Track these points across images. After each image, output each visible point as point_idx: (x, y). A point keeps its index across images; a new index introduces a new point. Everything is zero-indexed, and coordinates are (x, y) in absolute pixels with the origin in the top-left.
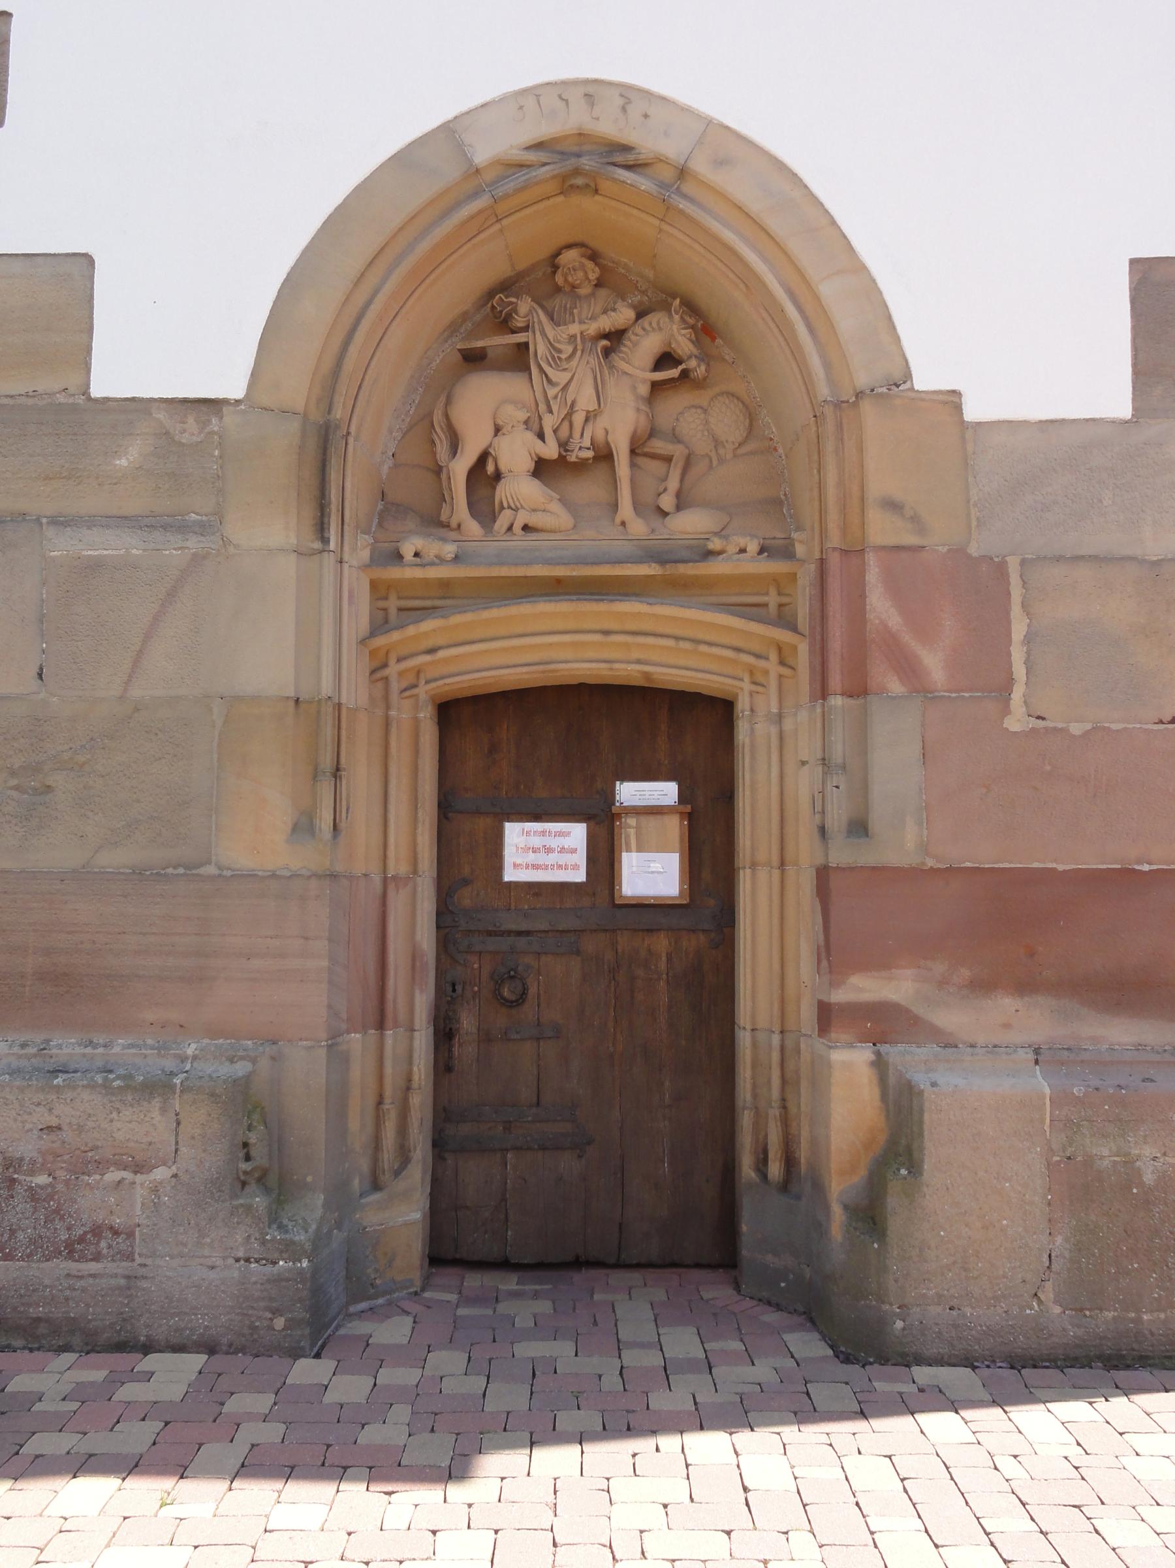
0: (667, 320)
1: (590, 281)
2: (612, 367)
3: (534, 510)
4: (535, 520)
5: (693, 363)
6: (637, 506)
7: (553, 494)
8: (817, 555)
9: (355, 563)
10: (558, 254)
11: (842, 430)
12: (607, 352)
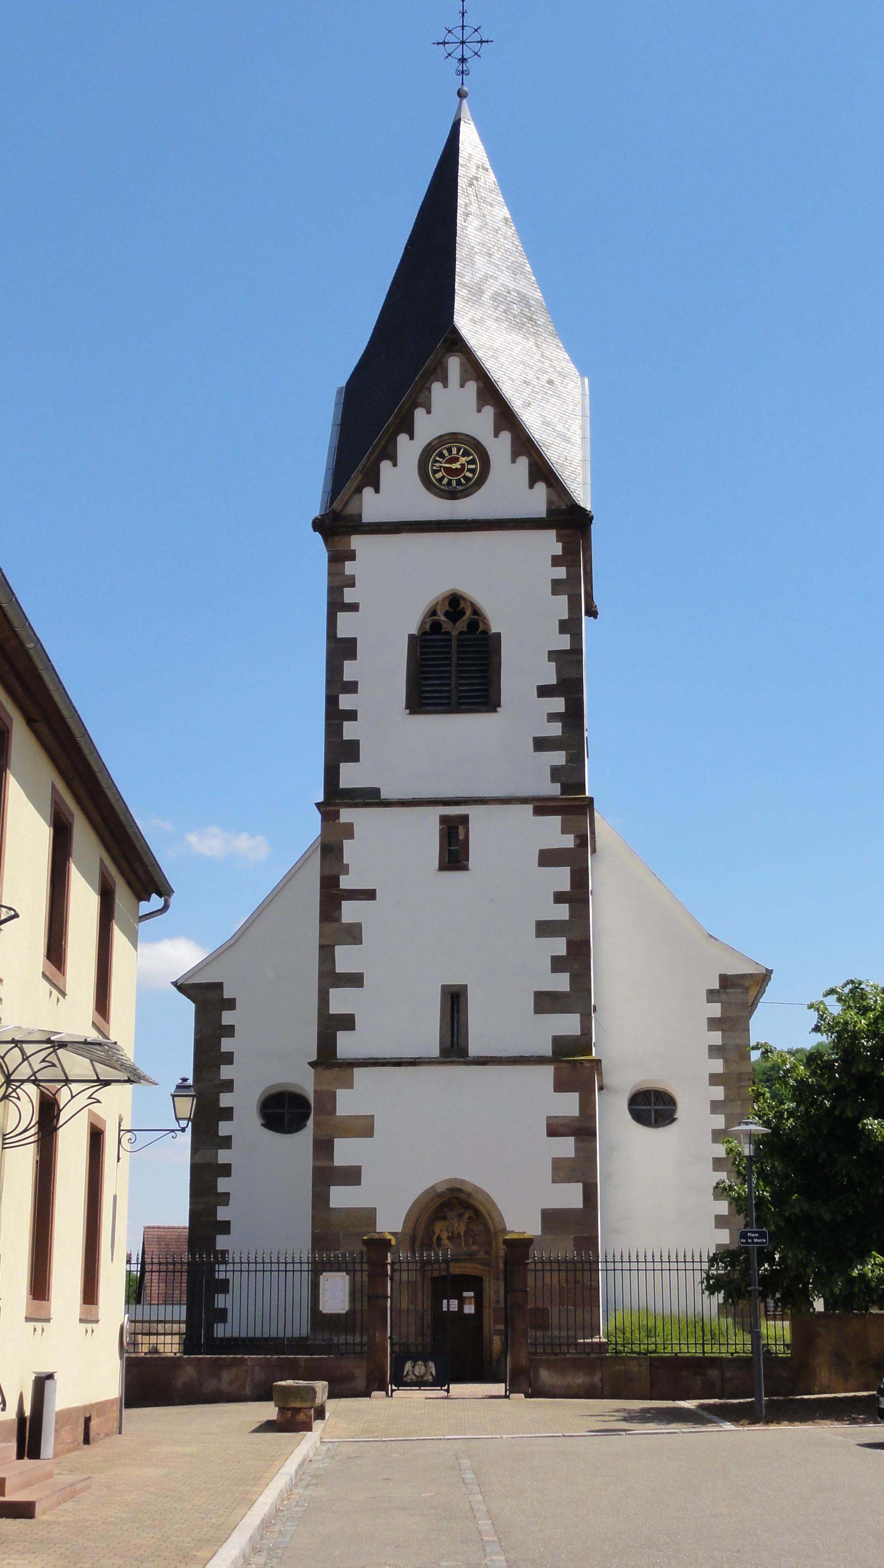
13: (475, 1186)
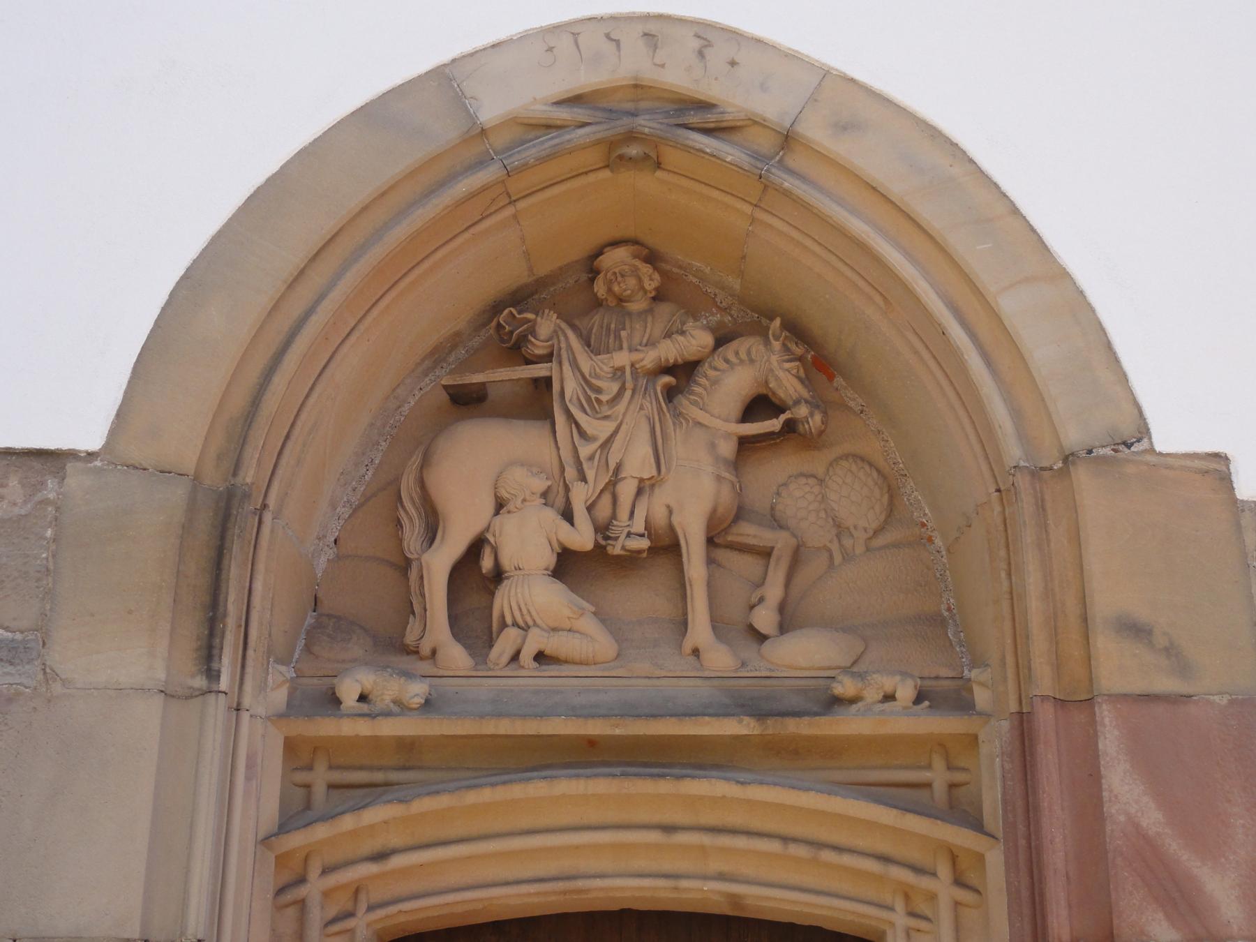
0: (762, 347)
1: (646, 292)
2: (678, 415)
3: (555, 630)
4: (553, 644)
5: (803, 411)
6: (718, 625)
7: (585, 604)
8: (1013, 707)
9: (261, 711)
10: (599, 253)
11: (1044, 510)
12: (671, 394)
13: (828, 79)
